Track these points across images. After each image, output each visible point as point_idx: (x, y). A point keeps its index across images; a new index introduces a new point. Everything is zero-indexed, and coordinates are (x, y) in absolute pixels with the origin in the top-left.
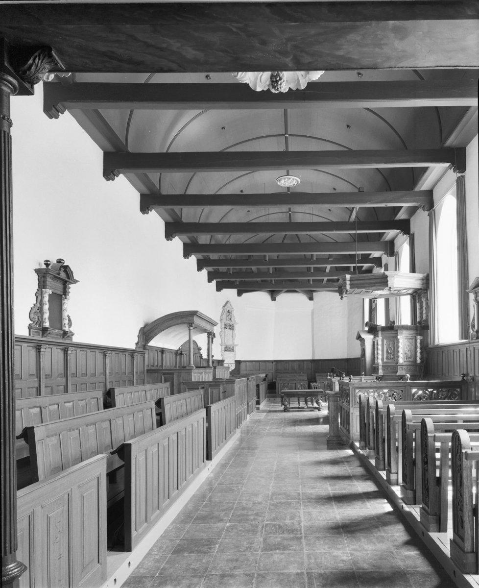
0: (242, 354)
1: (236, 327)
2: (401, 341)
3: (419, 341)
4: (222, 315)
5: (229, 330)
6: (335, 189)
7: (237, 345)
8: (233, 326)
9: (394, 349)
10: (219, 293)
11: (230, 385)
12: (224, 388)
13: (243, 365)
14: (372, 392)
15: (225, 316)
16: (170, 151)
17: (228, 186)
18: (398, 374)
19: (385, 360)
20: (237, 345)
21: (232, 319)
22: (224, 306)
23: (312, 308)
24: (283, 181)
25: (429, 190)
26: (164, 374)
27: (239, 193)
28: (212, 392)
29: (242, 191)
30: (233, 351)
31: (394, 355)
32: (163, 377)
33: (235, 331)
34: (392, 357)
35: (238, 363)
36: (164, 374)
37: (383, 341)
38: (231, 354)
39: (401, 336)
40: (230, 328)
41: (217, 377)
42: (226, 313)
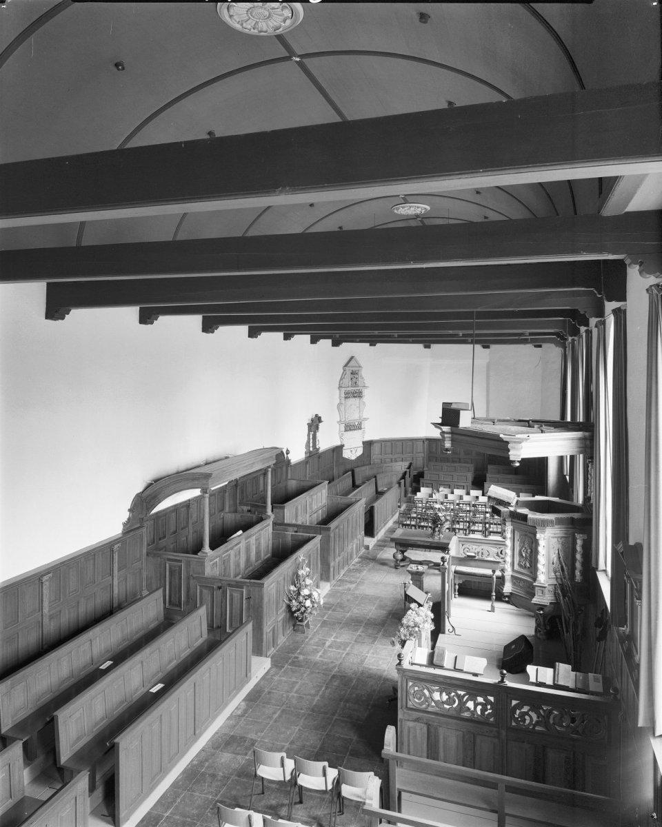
0: (373, 432)
1: (366, 392)
2: (542, 543)
3: (579, 542)
4: (341, 379)
5: (354, 399)
6: (486, 218)
7: (366, 419)
8: (361, 392)
9: (531, 552)
10: (335, 348)
11: (257, 589)
12: (249, 592)
13: (376, 450)
14: (437, 691)
15: (347, 381)
16: (179, 238)
17: (316, 225)
18: (535, 600)
19: (516, 567)
20: (366, 419)
21: (359, 383)
22: (346, 366)
23: (488, 361)
24: (398, 209)
25: (658, 210)
26: (169, 560)
27: (337, 229)
28: (231, 595)
29: (340, 228)
30: (361, 429)
31: (531, 563)
32: (167, 565)
33: (364, 399)
34: (528, 565)
35: (368, 445)
36: (169, 560)
37: (514, 534)
38: (356, 433)
39: (542, 535)
40: (354, 397)
41: (285, 522)
42: (348, 375)
